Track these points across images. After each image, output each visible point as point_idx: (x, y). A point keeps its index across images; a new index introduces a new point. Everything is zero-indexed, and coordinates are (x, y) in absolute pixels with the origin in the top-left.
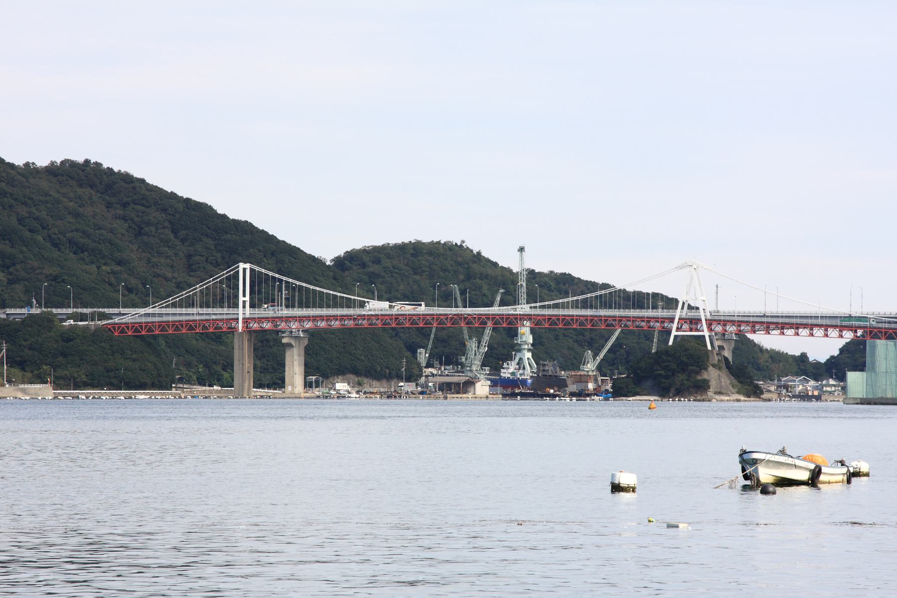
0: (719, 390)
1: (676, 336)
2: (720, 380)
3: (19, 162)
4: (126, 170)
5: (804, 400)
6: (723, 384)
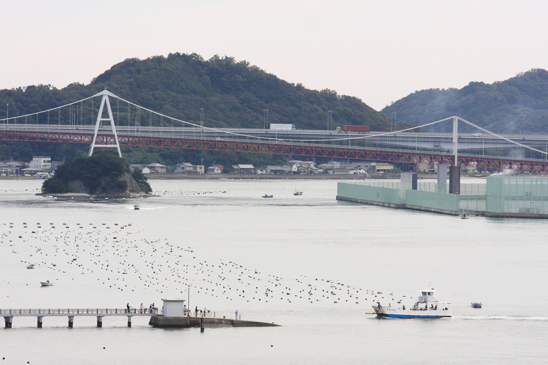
0: (132, 189)
1: (95, 148)
2: (131, 181)
3: (282, 79)
4: (293, 82)
5: (235, 198)
6: (134, 184)
